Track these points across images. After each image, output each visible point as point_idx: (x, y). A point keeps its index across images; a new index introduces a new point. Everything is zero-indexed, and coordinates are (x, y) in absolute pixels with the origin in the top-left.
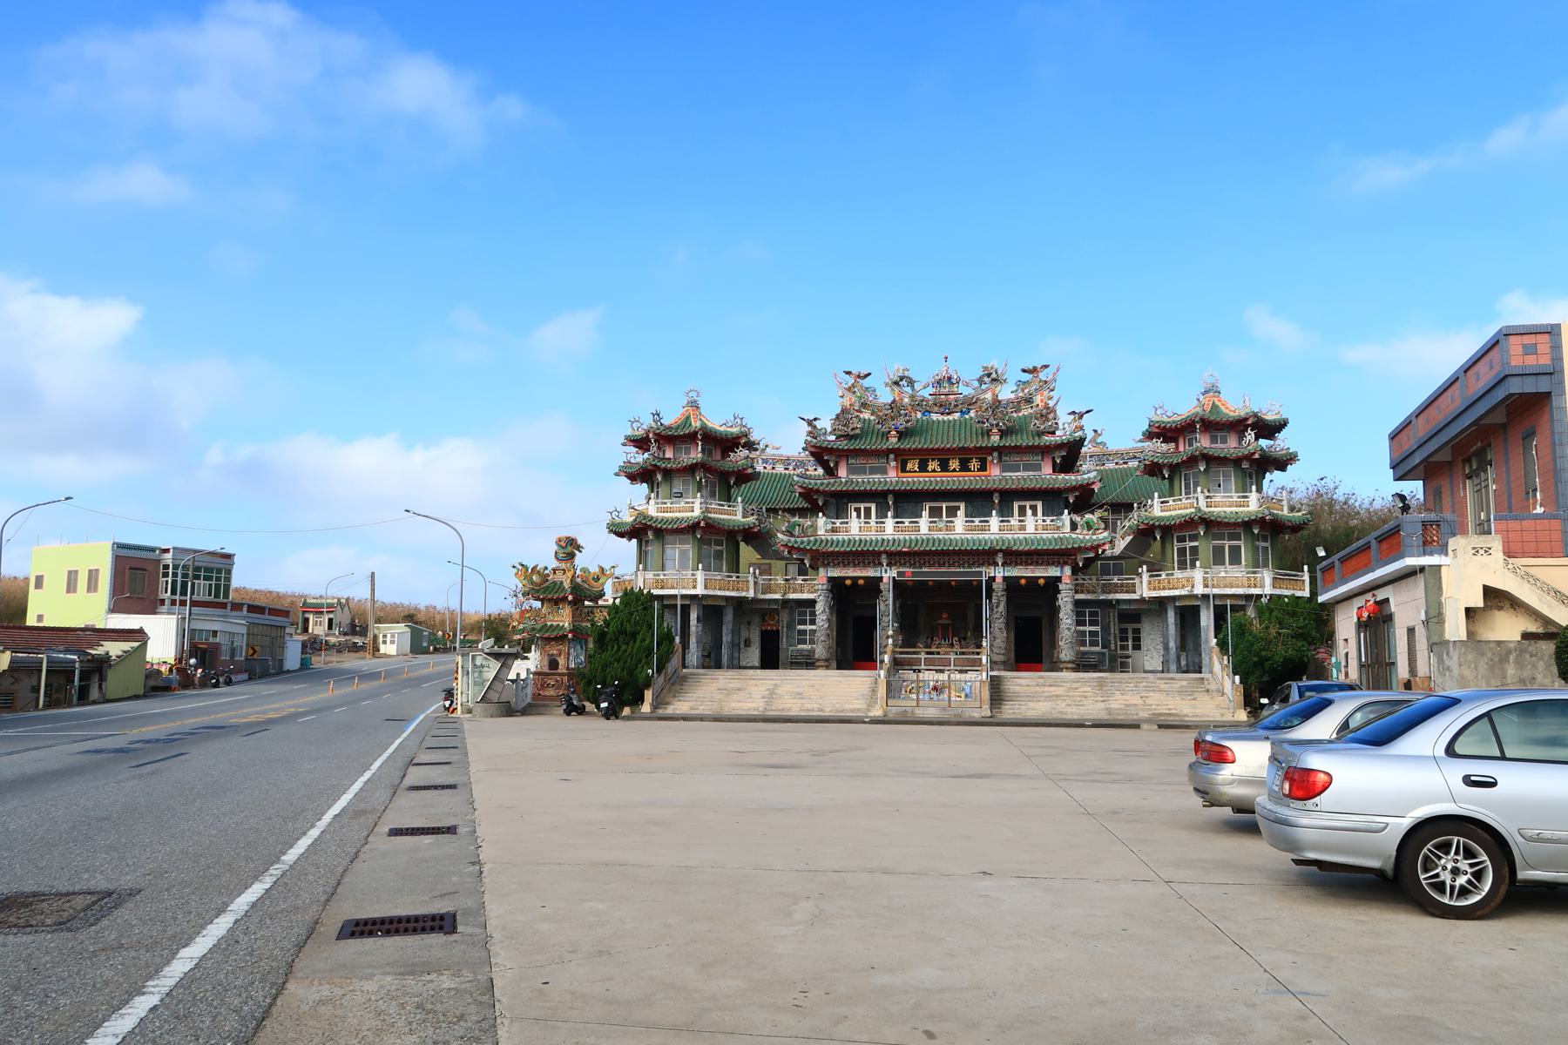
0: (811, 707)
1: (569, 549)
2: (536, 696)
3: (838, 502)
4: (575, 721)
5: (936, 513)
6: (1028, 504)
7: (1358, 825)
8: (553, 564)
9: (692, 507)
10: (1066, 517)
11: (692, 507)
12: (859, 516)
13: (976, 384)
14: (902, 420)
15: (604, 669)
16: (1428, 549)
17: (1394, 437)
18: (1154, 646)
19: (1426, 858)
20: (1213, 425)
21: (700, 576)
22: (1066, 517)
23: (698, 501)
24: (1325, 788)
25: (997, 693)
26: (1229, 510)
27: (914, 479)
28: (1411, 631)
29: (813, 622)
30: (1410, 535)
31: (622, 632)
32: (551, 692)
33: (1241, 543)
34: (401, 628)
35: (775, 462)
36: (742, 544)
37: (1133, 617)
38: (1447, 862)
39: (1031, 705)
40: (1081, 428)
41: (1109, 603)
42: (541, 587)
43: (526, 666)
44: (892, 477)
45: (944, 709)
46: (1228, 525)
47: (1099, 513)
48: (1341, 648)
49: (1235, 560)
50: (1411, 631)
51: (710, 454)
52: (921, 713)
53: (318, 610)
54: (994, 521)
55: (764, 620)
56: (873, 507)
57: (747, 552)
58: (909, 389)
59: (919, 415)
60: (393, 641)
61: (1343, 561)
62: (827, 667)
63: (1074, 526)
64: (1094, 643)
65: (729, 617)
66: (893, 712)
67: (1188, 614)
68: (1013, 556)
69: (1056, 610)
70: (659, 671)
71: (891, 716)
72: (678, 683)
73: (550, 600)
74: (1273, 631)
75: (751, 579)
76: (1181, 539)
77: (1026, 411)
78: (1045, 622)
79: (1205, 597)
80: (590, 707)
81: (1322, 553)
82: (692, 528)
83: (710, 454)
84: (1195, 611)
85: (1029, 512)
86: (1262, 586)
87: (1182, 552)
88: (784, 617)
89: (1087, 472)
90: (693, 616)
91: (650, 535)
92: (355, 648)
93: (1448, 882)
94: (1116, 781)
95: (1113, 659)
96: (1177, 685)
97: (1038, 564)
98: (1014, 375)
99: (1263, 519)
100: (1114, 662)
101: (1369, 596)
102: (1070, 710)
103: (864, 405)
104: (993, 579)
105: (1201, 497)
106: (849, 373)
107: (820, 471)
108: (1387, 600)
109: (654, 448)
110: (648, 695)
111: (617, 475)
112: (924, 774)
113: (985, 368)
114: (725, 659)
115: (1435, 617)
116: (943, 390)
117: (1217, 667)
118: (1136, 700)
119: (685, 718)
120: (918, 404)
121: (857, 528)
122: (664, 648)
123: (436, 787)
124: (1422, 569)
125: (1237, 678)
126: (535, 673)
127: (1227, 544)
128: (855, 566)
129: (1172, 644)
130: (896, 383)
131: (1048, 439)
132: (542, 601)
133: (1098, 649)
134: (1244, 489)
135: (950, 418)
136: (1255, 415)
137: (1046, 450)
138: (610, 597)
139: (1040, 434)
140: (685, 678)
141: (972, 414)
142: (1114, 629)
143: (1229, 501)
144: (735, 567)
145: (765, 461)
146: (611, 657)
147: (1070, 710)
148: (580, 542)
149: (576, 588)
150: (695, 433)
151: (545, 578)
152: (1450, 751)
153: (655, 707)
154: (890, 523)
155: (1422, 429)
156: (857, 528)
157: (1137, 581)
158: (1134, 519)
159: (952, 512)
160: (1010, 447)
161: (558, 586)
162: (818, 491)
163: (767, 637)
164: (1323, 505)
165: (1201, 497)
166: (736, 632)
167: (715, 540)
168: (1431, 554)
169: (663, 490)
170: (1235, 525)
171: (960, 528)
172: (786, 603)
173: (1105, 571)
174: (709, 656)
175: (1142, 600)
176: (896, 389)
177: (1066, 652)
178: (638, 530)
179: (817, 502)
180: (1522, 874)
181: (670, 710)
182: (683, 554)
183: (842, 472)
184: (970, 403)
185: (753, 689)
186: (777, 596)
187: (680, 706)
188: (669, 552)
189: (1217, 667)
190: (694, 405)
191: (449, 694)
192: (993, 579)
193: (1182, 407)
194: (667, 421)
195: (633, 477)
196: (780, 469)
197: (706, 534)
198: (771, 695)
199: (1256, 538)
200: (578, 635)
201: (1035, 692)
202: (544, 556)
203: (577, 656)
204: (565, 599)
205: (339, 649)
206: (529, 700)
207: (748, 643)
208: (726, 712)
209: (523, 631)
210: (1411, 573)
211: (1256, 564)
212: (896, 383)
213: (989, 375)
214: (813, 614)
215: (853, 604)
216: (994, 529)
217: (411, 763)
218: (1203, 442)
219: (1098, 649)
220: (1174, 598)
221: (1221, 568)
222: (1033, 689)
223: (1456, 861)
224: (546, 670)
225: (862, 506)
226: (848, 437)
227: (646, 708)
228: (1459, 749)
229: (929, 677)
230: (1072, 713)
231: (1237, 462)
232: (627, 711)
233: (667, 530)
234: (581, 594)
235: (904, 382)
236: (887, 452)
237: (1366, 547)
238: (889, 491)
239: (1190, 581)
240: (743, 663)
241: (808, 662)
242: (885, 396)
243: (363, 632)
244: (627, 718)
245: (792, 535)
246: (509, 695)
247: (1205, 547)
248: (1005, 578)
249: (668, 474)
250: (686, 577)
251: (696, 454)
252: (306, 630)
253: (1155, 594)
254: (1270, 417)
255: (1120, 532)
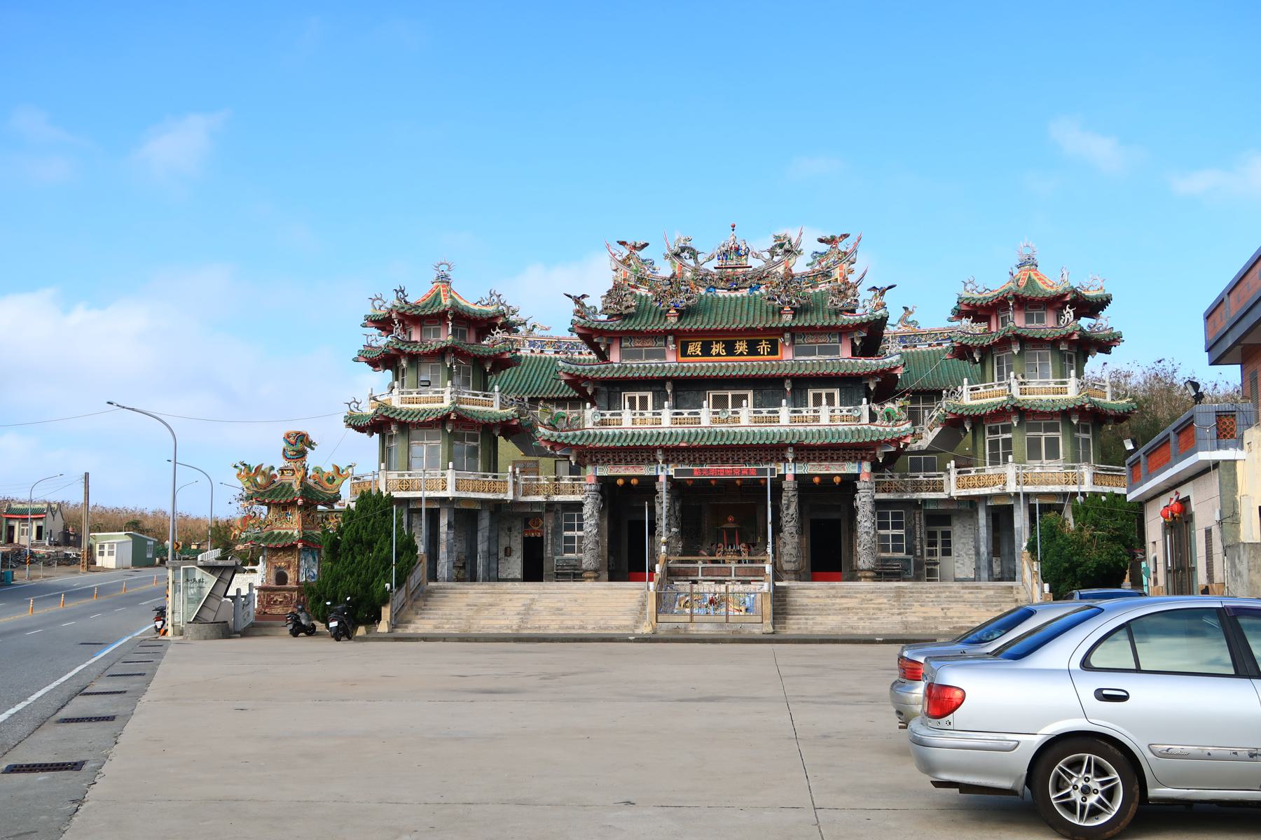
0: (572, 623)
1: (299, 446)
2: (262, 615)
3: (609, 391)
4: (303, 642)
5: (720, 402)
6: (824, 392)
7: (989, 744)
8: (280, 463)
9: (441, 397)
10: (864, 407)
11: (441, 397)
12: (632, 407)
13: (767, 255)
14: (682, 297)
15: (334, 583)
16: (1223, 441)
17: (1208, 316)
18: (967, 548)
19: (1058, 778)
20: (1028, 302)
21: (450, 476)
22: (864, 407)
23: (448, 390)
24: (958, 706)
25: (781, 605)
26: (1044, 397)
27: (697, 364)
28: (1208, 532)
29: (580, 528)
30: (1203, 427)
31: (358, 540)
32: (279, 610)
33: (1059, 435)
34: (121, 537)
35: (544, 344)
36: (501, 439)
37: (941, 519)
38: (1078, 780)
39: (819, 619)
40: (883, 306)
41: (914, 504)
42: (266, 490)
43: (249, 582)
44: (670, 361)
45: (720, 624)
46: (1044, 414)
47: (900, 402)
48: (1151, 555)
49: (1053, 453)
50: (1208, 532)
51: (463, 336)
52: (694, 629)
53: (23, 516)
54: (785, 412)
55: (526, 525)
56: (650, 395)
57: (507, 449)
58: (691, 262)
59: (703, 292)
60: (112, 552)
61: (1148, 454)
62: (597, 579)
63: (873, 417)
64: (897, 549)
65: (484, 522)
66: (663, 630)
67: (1001, 516)
68: (805, 451)
69: (853, 512)
70: (399, 584)
71: (661, 633)
72: (421, 598)
73: (277, 505)
74: (1087, 534)
75: (510, 479)
76: (994, 431)
77: (823, 287)
78: (844, 526)
79: (1017, 495)
80: (320, 626)
81: (1130, 447)
82: (442, 421)
83: (463, 336)
84: (1009, 510)
85: (824, 401)
86: (1082, 483)
87: (994, 445)
88: (549, 523)
89: (892, 356)
90: (444, 522)
91: (394, 428)
92: (67, 561)
93: (1079, 801)
94: (857, 703)
95: (919, 566)
96: (982, 595)
97: (832, 460)
98: (810, 245)
99: (1082, 407)
100: (925, 571)
101: (1172, 494)
102: (861, 624)
103: (641, 280)
104: (783, 477)
105: (1014, 384)
106: (623, 243)
107: (594, 356)
108: (1187, 499)
109: (397, 329)
110: (386, 612)
111: (356, 360)
112: (651, 698)
113: (777, 238)
114: (480, 570)
115: (1230, 517)
116: (730, 263)
117: (1027, 574)
118: (935, 612)
119: (425, 638)
120: (702, 278)
121: (633, 420)
122: (404, 559)
123: (90, 719)
124: (1216, 465)
125: (1046, 586)
126: (260, 589)
127: (1043, 436)
128: (627, 463)
129: (983, 549)
130: (677, 255)
131: (846, 318)
132: (269, 505)
133: (902, 555)
134: (1063, 374)
135: (738, 294)
136: (1074, 291)
137: (843, 331)
138: (347, 497)
139: (838, 313)
140: (429, 594)
141: (763, 290)
142: (921, 532)
143: (1045, 387)
144: (492, 464)
145: (532, 344)
146: (346, 569)
147: (861, 624)
148: (311, 438)
149: (306, 490)
150: (445, 313)
151: (271, 479)
152: (1085, 664)
153: (394, 625)
154: (667, 414)
155: (1233, 308)
156: (633, 420)
157: (945, 478)
158: (946, 403)
159: (738, 401)
160: (803, 328)
161: (286, 488)
162: (586, 378)
163: (525, 542)
164: (1161, 389)
165: (1014, 384)
166: (493, 540)
167: (471, 436)
168: (1226, 448)
169: (410, 377)
170: (1052, 414)
171: (746, 420)
172: (550, 506)
173: (916, 467)
174: (463, 567)
175: (950, 500)
176: (677, 262)
177: (864, 560)
178: (381, 425)
179: (586, 390)
180: (1155, 792)
181: (411, 630)
182: (432, 450)
183: (615, 356)
184: (760, 277)
185: (510, 603)
186: (540, 498)
187: (422, 625)
188: (415, 448)
189: (1027, 574)
190: (444, 280)
191: (161, 614)
192: (783, 477)
193: (994, 281)
194: (412, 299)
195: (374, 363)
196: (549, 353)
197: (456, 426)
198: (528, 610)
199: (1076, 429)
200: (309, 545)
201: (826, 604)
202: (273, 457)
203: (309, 569)
204: (294, 503)
205: (48, 562)
206: (251, 619)
207: (508, 552)
208: (474, 631)
209: (245, 540)
210: (1205, 470)
211: (1076, 458)
212: (677, 255)
213: (781, 246)
214: (581, 518)
215: (624, 506)
216: (785, 420)
217: (82, 692)
218: (1018, 321)
219: (902, 555)
220: (985, 498)
221: (1037, 463)
222: (820, 601)
223: (1087, 780)
224: (273, 584)
225: (637, 395)
226: (620, 316)
227: (383, 627)
228: (1095, 661)
229: (708, 588)
230: (863, 627)
231: (1054, 343)
232: (361, 631)
233: (413, 424)
234: (313, 498)
235: (685, 254)
236: (668, 333)
237: (1165, 441)
238: (666, 379)
239: (1002, 478)
240: (502, 575)
241: (574, 574)
242: (665, 270)
243: (77, 543)
244: (362, 639)
245: (555, 429)
246: (226, 614)
247: (1019, 439)
248: (796, 476)
249: (414, 359)
250: (435, 476)
251: (446, 337)
252: (10, 539)
253: (964, 492)
254: (1091, 293)
255: (927, 423)
